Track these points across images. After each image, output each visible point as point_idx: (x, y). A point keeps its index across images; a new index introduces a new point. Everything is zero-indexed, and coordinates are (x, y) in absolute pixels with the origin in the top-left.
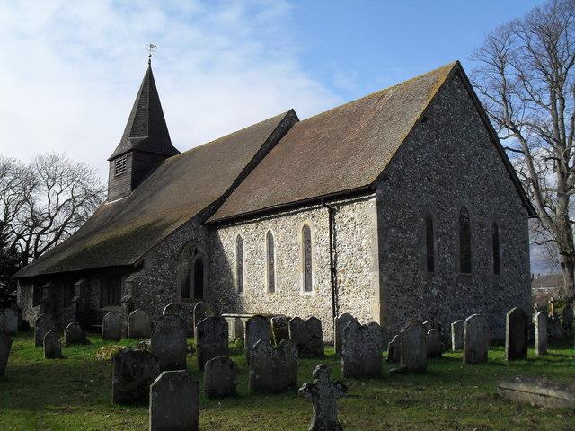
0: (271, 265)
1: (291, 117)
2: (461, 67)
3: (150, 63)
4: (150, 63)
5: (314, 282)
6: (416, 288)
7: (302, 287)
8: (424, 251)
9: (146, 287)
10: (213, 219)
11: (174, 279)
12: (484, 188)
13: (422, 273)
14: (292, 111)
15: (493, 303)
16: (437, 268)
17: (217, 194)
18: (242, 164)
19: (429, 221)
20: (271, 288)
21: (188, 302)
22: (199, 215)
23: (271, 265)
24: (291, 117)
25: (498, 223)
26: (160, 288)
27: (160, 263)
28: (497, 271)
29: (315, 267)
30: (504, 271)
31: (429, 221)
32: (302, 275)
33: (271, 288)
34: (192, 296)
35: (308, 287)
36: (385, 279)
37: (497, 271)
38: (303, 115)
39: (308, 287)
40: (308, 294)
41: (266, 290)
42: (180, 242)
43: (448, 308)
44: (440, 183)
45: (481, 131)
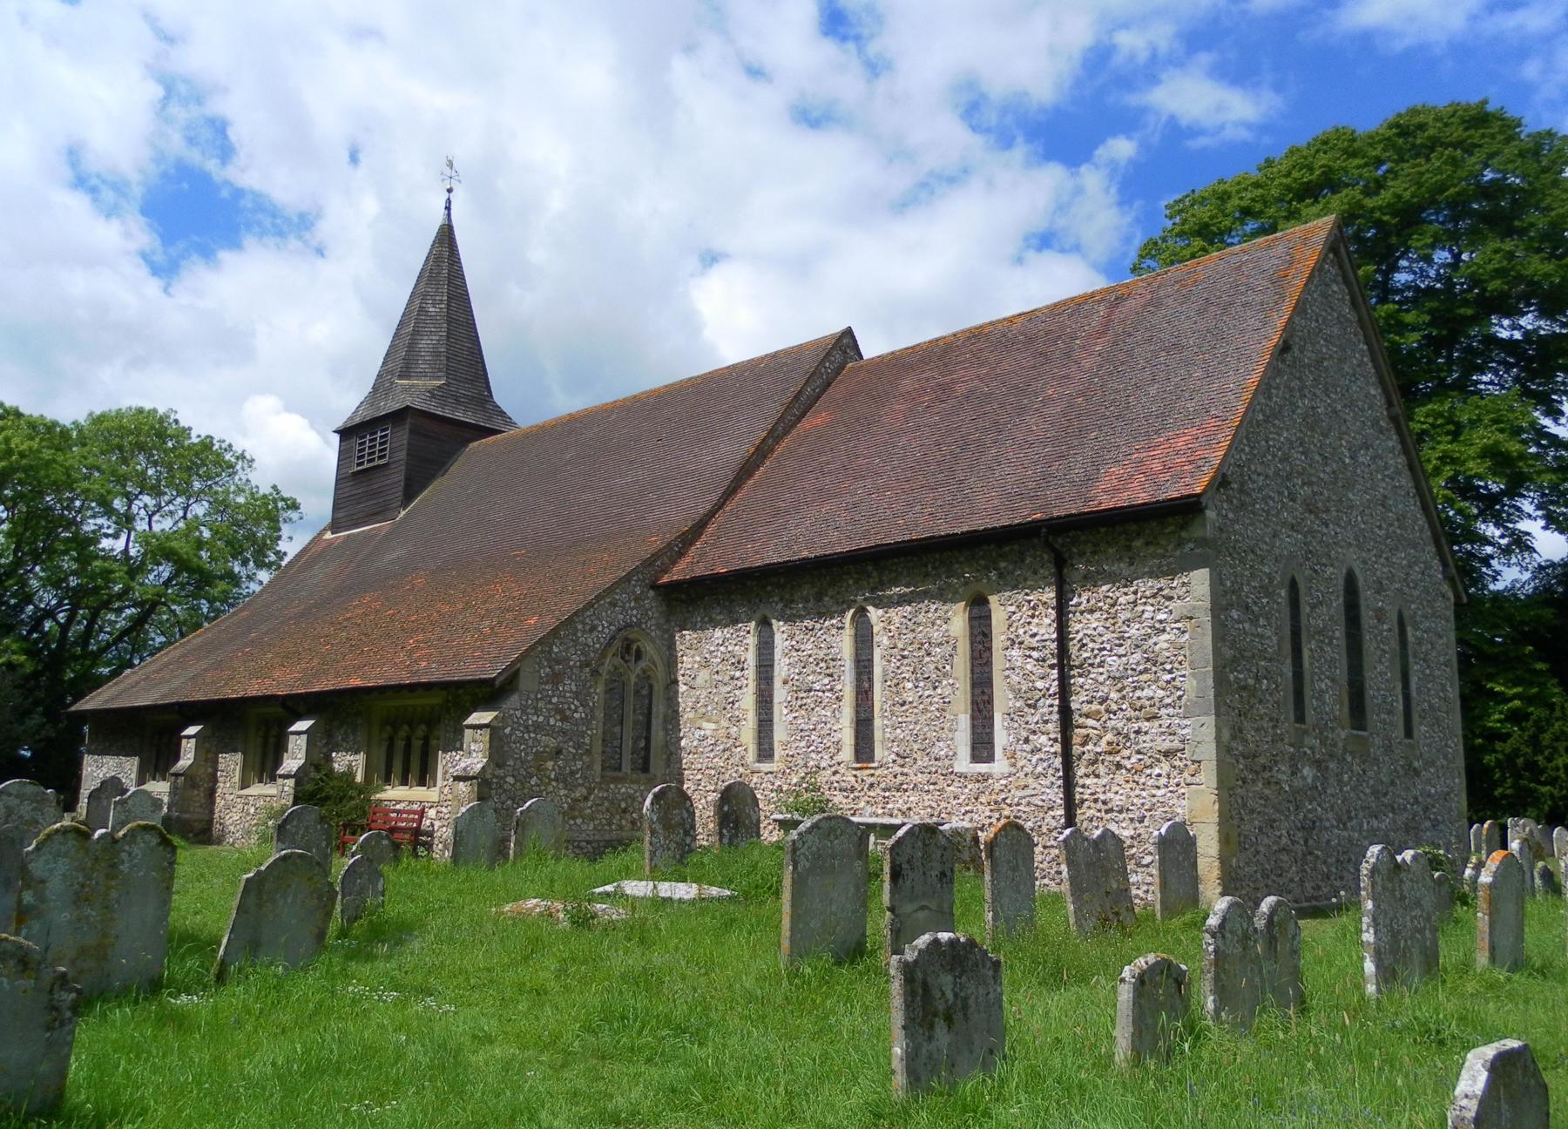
0: (864, 695)
1: (846, 342)
2: (853, 337)
3: (448, 208)
4: (448, 208)
5: (1001, 738)
6: (1276, 763)
7: (964, 751)
8: (1288, 670)
9: (522, 740)
10: (680, 571)
11: (587, 721)
12: (1380, 527)
13: (1287, 725)
14: (849, 332)
15: (1405, 809)
16: (1311, 715)
17: (680, 516)
18: (735, 449)
19: (1293, 586)
20: (864, 749)
21: (616, 780)
22: (648, 563)
23: (864, 695)
24: (846, 342)
25: (1406, 614)
26: (553, 743)
27: (556, 679)
28: (1409, 732)
29: (1003, 700)
30: (1421, 729)
31: (1293, 586)
32: (964, 721)
33: (864, 749)
34: (626, 767)
35: (982, 748)
36: (1226, 735)
37: (1409, 732)
38: (872, 347)
39: (982, 748)
40: (982, 768)
41: (847, 754)
42: (605, 629)
43: (1330, 815)
44: (1310, 509)
45: (1373, 392)
